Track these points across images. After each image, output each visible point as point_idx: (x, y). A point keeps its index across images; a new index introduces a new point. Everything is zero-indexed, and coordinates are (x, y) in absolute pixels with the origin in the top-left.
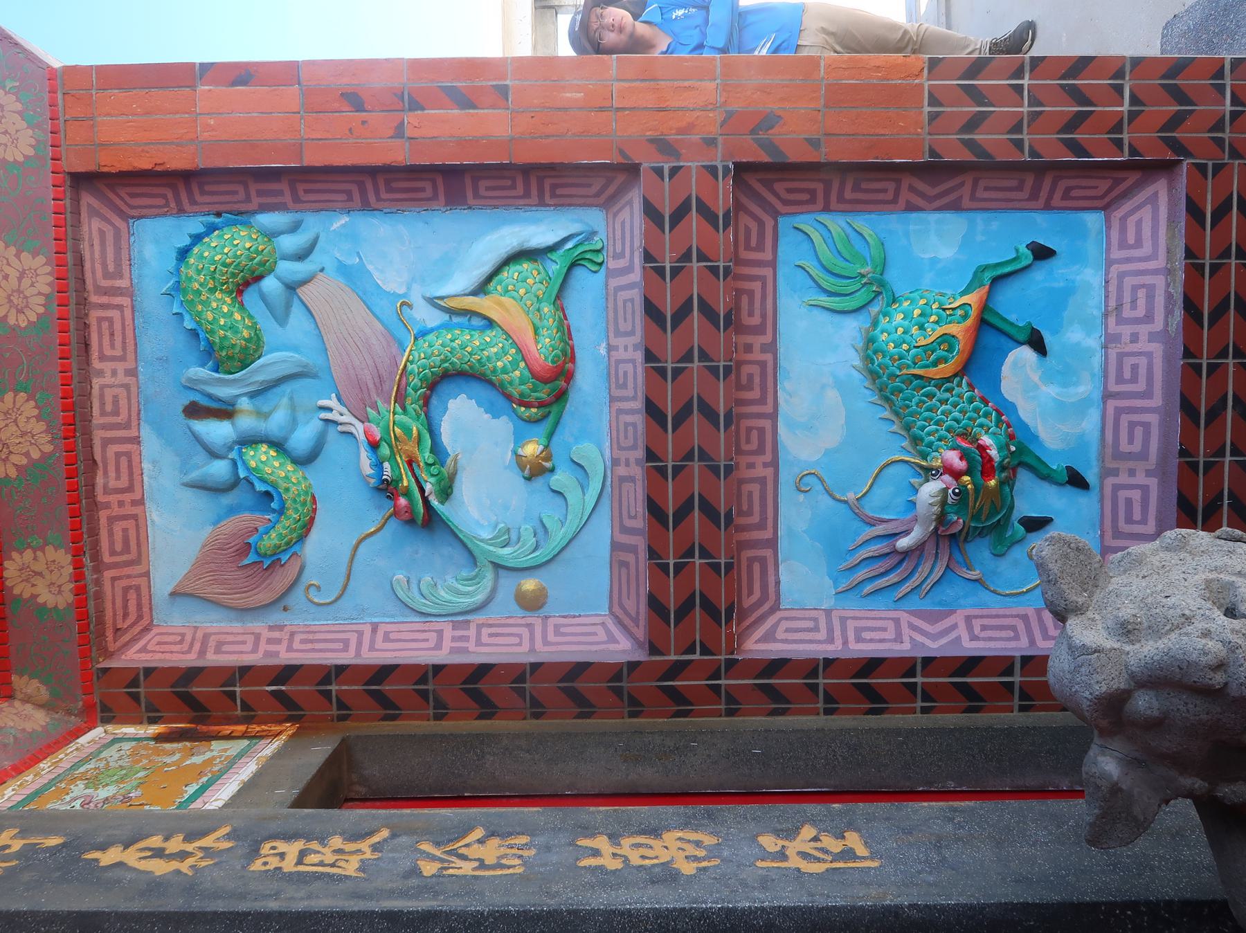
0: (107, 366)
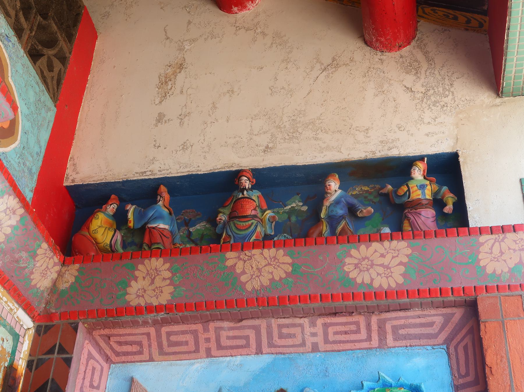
0: (319, 329)
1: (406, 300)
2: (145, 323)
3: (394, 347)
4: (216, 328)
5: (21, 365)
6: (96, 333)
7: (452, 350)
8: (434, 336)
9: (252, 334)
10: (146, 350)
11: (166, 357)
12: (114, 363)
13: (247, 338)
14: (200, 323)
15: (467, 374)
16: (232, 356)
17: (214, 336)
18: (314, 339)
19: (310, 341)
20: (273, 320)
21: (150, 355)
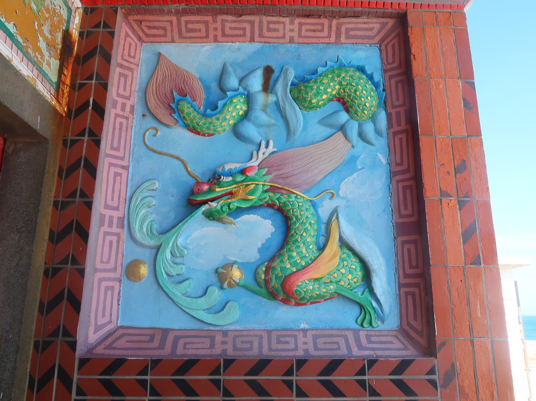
0: (296, 27)
1: (360, 9)
2: (170, 12)
3: (345, 43)
4: (222, 20)
5: (75, 34)
6: (131, 18)
7: (383, 47)
8: (373, 38)
9: (248, 26)
10: (169, 34)
11: (184, 40)
12: (145, 42)
13: (244, 29)
14: (212, 15)
15: (393, 62)
16: (232, 42)
17: (220, 27)
18: (292, 34)
19: (288, 34)
20: (264, 17)
21: (172, 38)
